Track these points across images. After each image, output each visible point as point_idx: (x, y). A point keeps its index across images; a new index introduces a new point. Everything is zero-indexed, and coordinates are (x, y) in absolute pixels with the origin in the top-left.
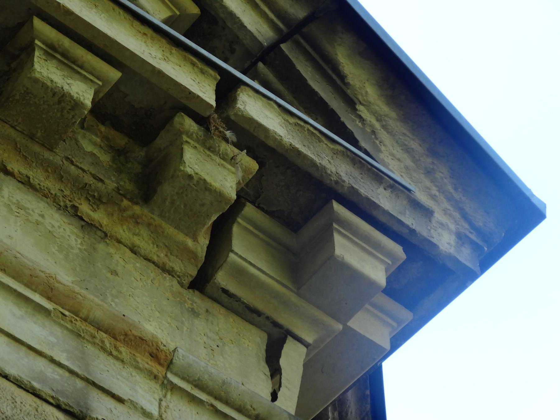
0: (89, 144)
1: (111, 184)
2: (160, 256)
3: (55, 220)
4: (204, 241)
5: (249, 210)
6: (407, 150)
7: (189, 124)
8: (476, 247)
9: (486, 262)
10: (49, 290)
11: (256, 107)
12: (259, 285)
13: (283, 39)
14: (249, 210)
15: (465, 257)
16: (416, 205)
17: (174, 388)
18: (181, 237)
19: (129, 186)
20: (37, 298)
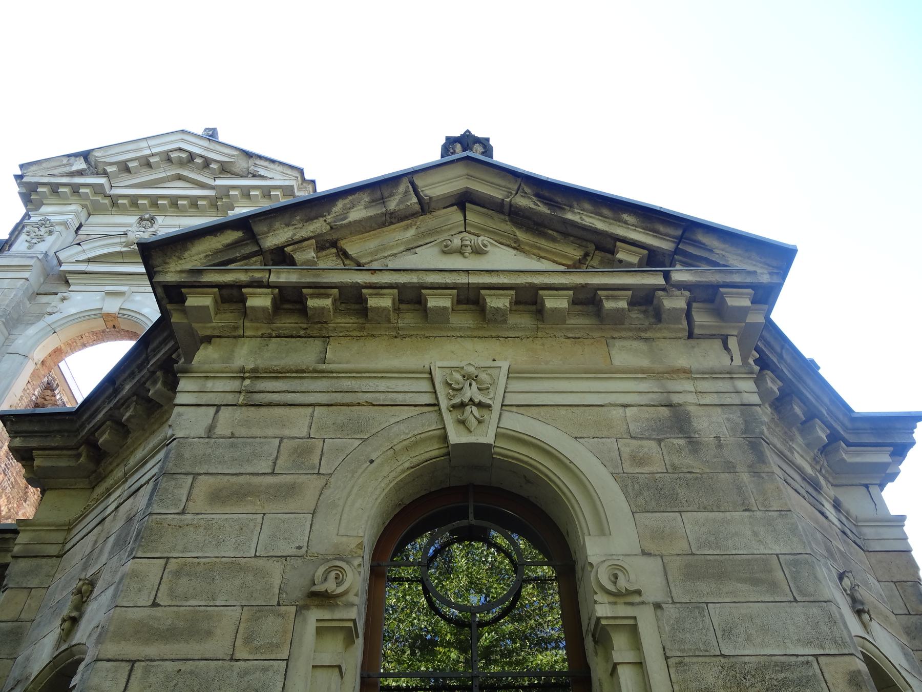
0: (634, 315)
1: (647, 323)
2: (673, 335)
3: (636, 344)
4: (685, 323)
5: (694, 305)
6: (738, 255)
7: (660, 293)
8: (778, 274)
9: (784, 278)
10: (643, 371)
11: (680, 275)
12: (710, 326)
13: (678, 244)
14: (694, 305)
15: (775, 280)
16: (749, 273)
17: (696, 378)
18: (677, 326)
19: (653, 320)
20: (640, 376)
